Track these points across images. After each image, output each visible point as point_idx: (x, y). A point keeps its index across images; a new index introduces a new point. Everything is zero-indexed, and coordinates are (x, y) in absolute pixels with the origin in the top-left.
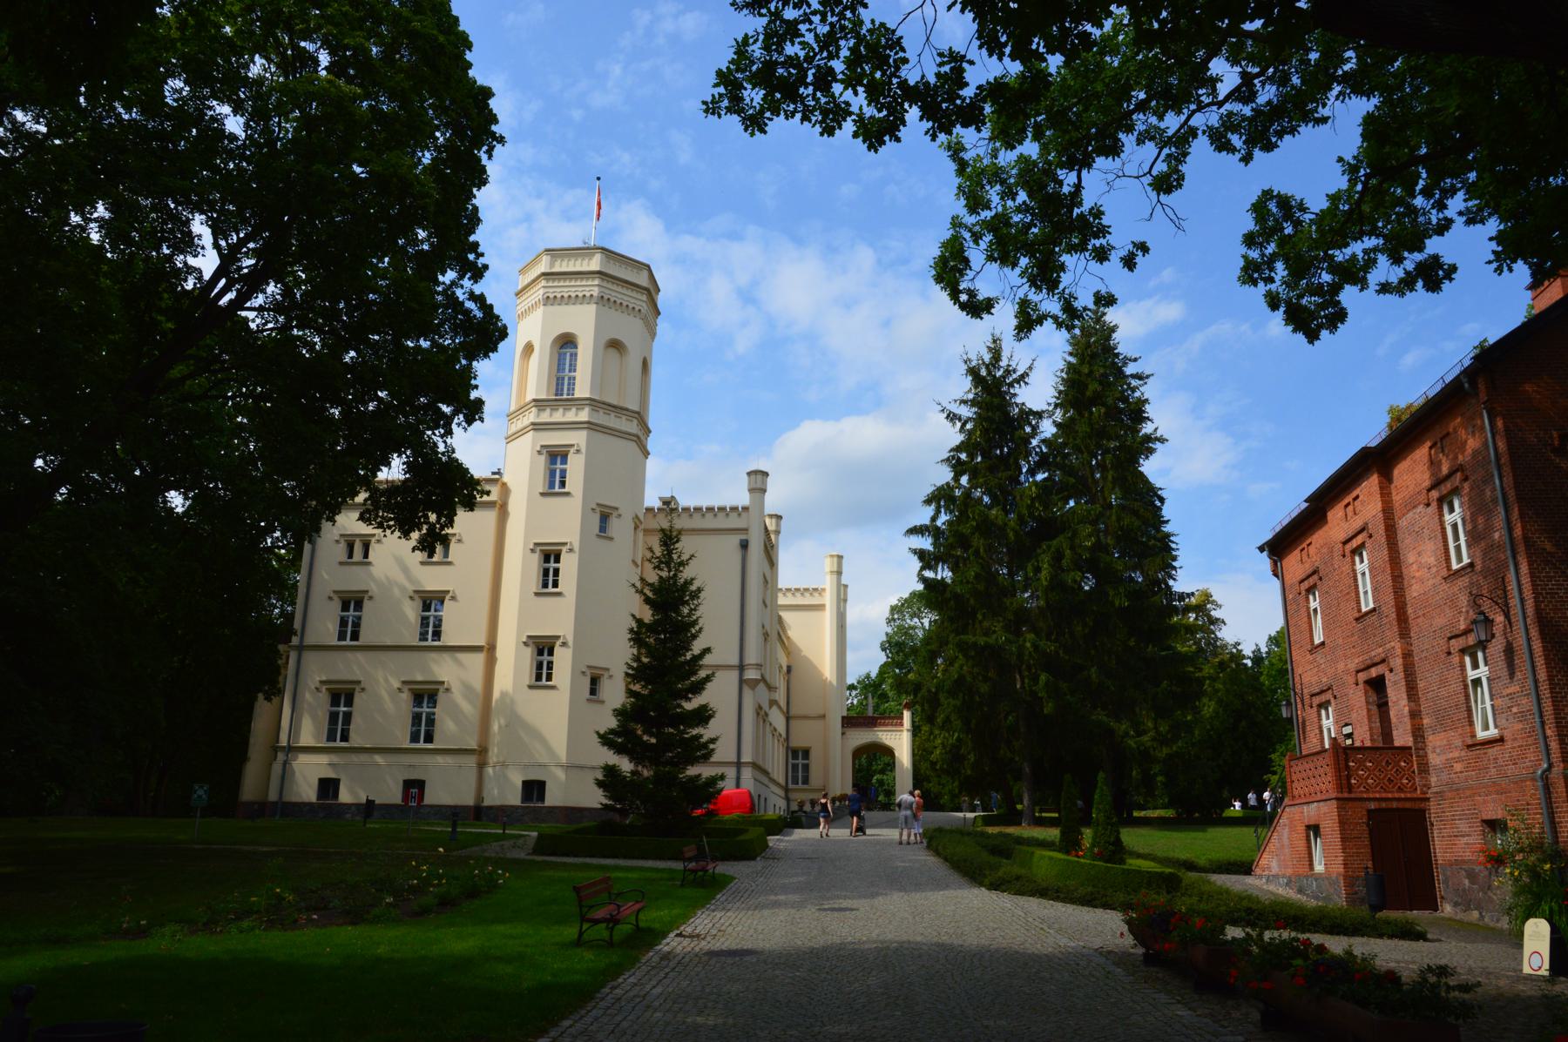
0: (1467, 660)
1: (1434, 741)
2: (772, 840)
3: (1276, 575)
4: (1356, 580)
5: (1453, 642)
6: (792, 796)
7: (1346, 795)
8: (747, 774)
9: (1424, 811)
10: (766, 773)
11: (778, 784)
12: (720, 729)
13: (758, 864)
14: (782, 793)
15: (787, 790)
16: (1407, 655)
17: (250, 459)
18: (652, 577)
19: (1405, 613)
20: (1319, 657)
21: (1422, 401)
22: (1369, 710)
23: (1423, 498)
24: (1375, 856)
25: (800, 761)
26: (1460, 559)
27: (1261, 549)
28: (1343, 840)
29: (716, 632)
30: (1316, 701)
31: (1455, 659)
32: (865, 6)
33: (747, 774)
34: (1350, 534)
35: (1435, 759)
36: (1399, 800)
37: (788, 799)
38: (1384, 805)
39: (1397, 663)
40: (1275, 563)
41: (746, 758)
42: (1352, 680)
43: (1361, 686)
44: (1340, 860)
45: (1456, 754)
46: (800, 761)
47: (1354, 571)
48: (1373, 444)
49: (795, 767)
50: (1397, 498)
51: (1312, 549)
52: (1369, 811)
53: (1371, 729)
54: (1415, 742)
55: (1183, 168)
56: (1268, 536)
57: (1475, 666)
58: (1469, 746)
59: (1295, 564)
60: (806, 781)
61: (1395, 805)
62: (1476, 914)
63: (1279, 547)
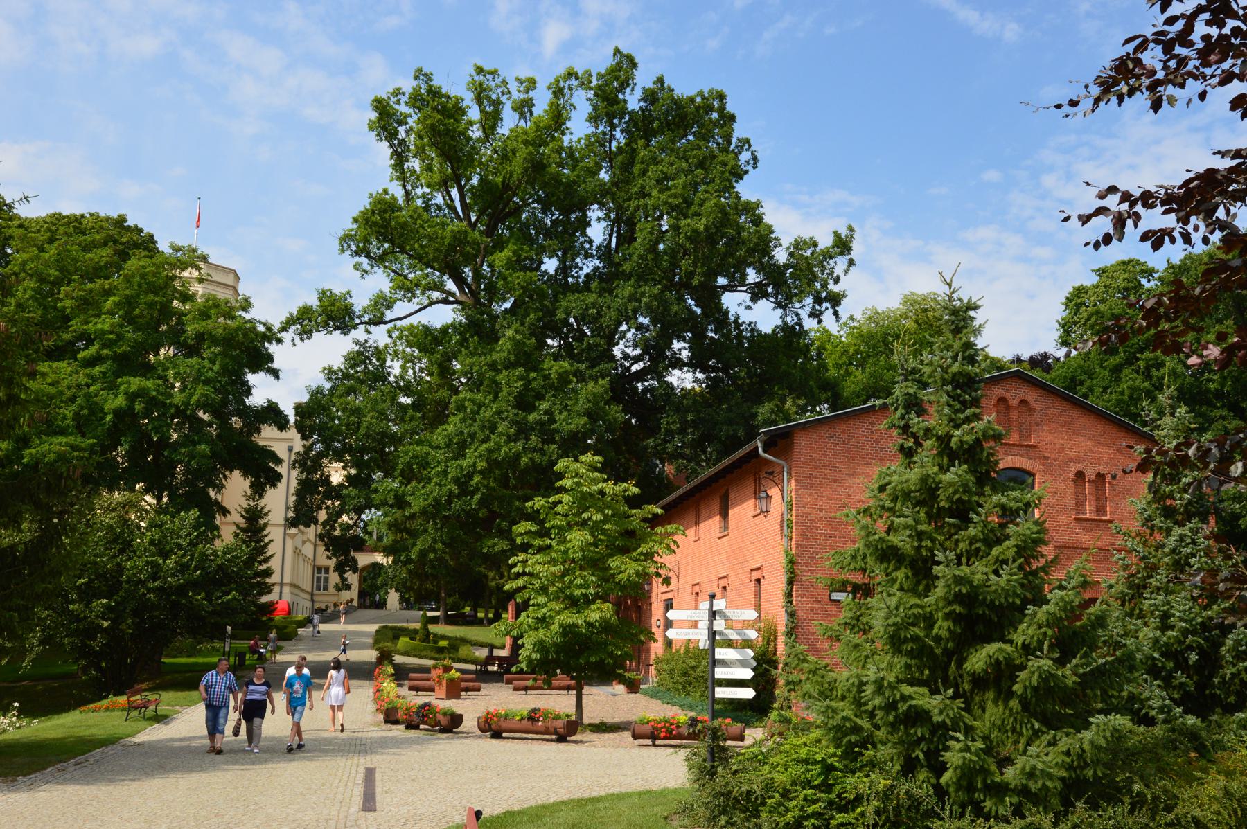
2: (300, 631)
6: (316, 598)
8: (286, 590)
10: (298, 587)
11: (304, 591)
12: (274, 564)
13: (293, 642)
14: (309, 597)
15: (312, 594)
17: (694, 134)
18: (245, 505)
25: (323, 575)
29: (110, 750)
32: (1243, 117)
33: (286, 590)
37: (313, 601)
41: (287, 580)
46: (323, 575)
49: (319, 579)
55: (1137, 193)
60: (326, 588)
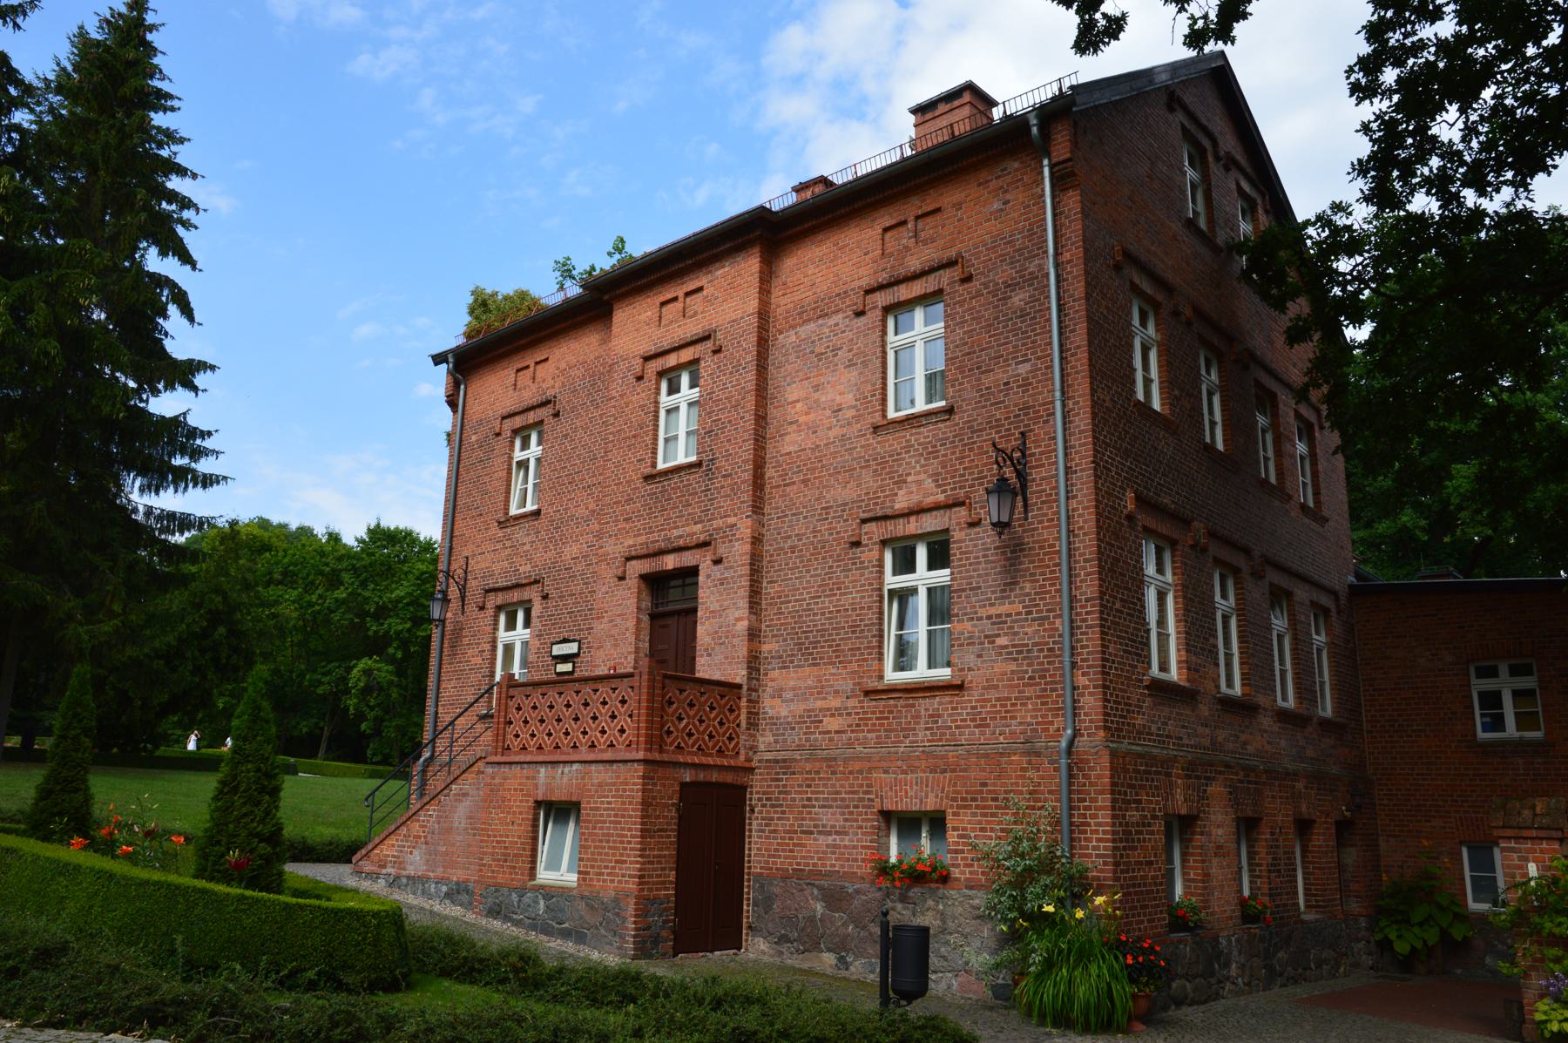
0: (502, 619)
1: (775, 677)
3: (452, 402)
4: (656, 417)
5: (491, 596)
7: (657, 756)
9: (743, 788)
16: (757, 540)
19: (763, 475)
20: (520, 534)
21: (848, 177)
22: (639, 621)
23: (856, 300)
24: (680, 868)
26: (523, 503)
27: (438, 359)
28: (645, 833)
30: (494, 600)
31: (868, 554)
34: (666, 345)
35: (772, 707)
36: (721, 768)
38: (701, 776)
39: (738, 551)
40: (457, 385)
42: (608, 573)
43: (632, 582)
44: (632, 868)
45: (835, 703)
47: (657, 403)
48: (776, 207)
50: (782, 301)
51: (549, 367)
52: (683, 785)
53: (637, 650)
54: (749, 679)
56: (435, 352)
57: (511, 626)
58: (867, 693)
59: (498, 390)
61: (715, 777)
62: (829, 959)
63: (496, 342)
